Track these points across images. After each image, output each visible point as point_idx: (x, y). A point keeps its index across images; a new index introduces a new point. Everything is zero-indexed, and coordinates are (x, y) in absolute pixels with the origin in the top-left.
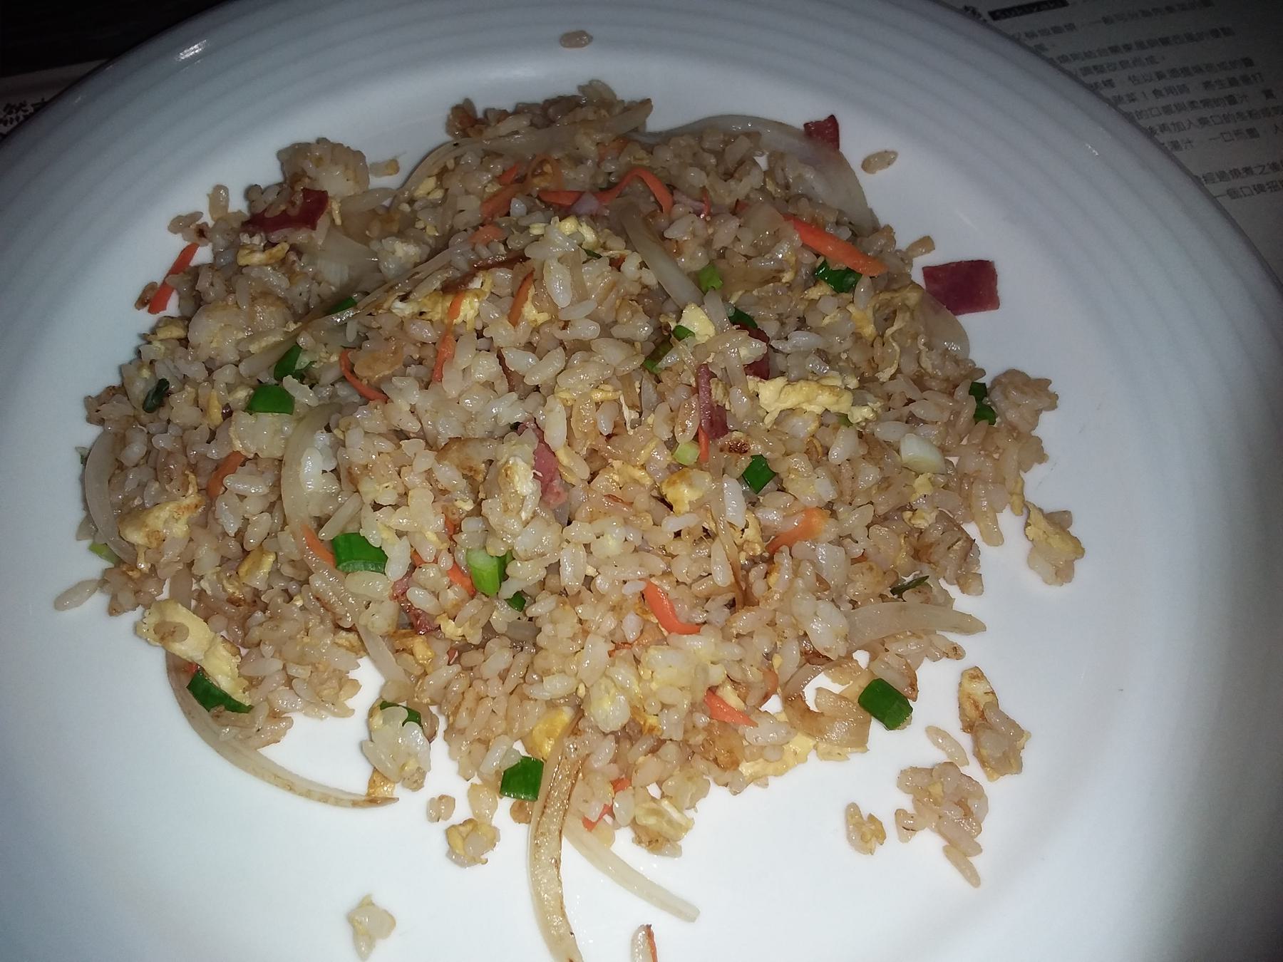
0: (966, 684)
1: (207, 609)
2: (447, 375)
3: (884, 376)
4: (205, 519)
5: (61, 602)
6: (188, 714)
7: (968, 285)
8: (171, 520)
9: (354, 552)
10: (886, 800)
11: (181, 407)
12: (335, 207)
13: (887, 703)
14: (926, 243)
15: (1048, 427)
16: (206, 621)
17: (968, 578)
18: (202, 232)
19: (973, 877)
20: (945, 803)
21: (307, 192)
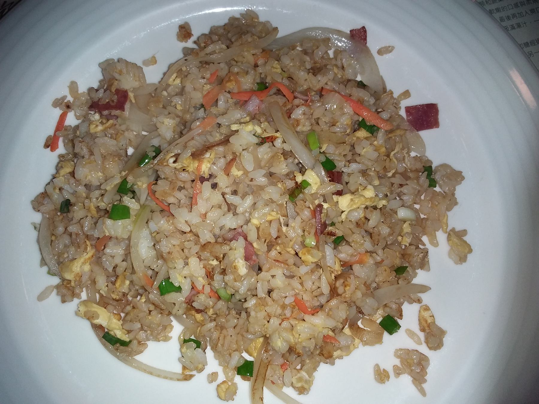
0: (422, 311)
1: (104, 303)
2: (200, 201)
3: (390, 174)
4: (97, 260)
5: (41, 297)
6: (104, 345)
7: (425, 116)
8: (81, 266)
9: (168, 287)
10: (389, 362)
11: (77, 212)
12: (131, 95)
13: (390, 325)
14: (406, 94)
15: (460, 192)
16: (105, 308)
17: (424, 264)
18: (68, 107)
19: (423, 393)
20: (414, 366)
21: (118, 91)
